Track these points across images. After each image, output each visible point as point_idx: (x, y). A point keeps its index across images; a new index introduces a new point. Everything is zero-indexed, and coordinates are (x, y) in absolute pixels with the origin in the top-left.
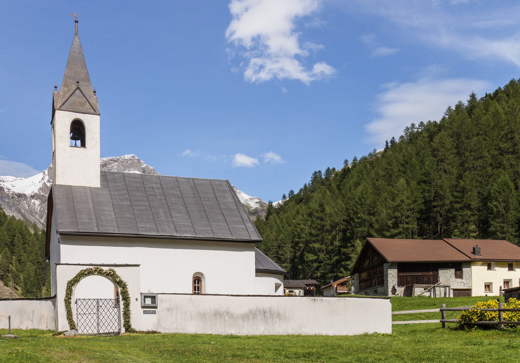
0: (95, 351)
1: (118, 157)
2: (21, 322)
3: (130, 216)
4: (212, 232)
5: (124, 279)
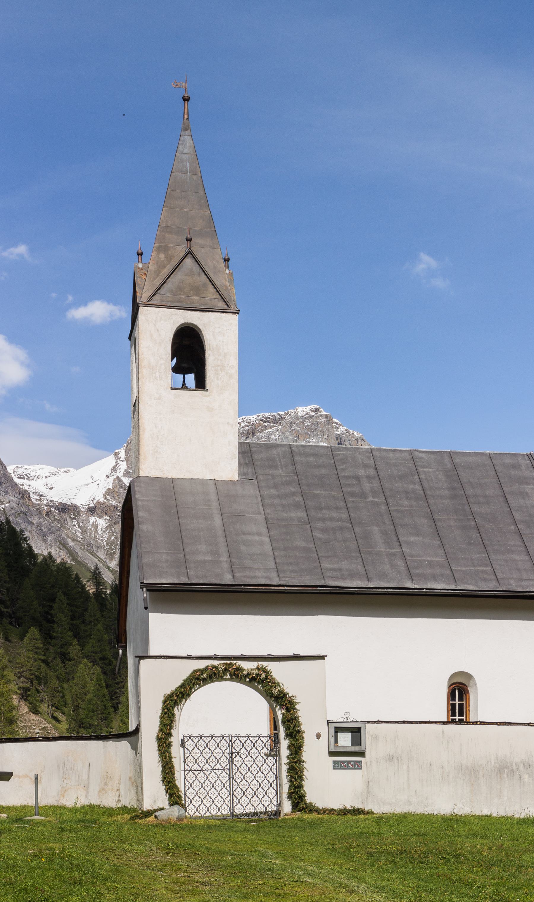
0: (223, 853)
1: (282, 413)
2: (64, 792)
3: (303, 544)
4: (493, 577)
5: (290, 689)
